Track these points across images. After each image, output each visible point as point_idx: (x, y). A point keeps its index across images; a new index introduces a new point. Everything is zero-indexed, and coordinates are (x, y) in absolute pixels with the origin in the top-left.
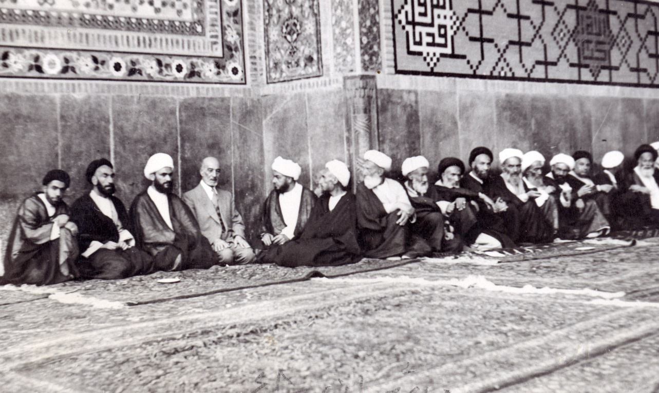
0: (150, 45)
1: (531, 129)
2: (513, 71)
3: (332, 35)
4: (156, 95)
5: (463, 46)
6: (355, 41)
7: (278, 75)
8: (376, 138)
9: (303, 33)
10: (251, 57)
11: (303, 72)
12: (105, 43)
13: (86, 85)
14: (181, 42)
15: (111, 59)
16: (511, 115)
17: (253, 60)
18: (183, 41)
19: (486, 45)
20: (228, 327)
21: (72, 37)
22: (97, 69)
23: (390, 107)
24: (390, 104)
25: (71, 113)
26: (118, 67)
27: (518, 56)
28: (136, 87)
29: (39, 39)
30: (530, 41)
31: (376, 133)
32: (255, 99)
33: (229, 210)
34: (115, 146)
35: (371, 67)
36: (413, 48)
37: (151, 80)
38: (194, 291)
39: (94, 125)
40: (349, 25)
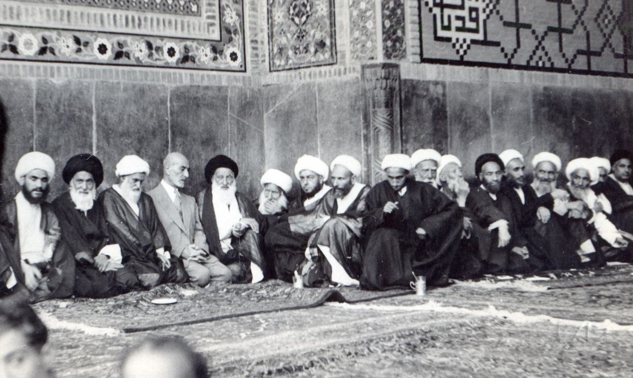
0: (139, 25)
1: (572, 129)
2: (552, 61)
3: (348, 17)
4: (144, 82)
5: (496, 30)
6: (376, 24)
7: (283, 63)
8: (399, 136)
9: (314, 15)
10: (252, 41)
11: (313, 59)
12: (88, 22)
13: (66, 68)
14: (173, 23)
15: (95, 40)
16: (549, 112)
17: (254, 45)
18: (176, 21)
19: (524, 32)
20: (254, 363)
21: (52, 15)
22: (79, 51)
23: (414, 100)
24: (415, 97)
25: (49, 100)
26: (103, 49)
27: (557, 44)
28: (123, 71)
29: (15, 16)
30: (571, 28)
31: (399, 131)
32: (256, 90)
33: (193, 215)
34: (98, 140)
35: (394, 54)
36: (441, 33)
37: (139, 64)
38: (198, 316)
39: (74, 115)
40: (369, 7)
